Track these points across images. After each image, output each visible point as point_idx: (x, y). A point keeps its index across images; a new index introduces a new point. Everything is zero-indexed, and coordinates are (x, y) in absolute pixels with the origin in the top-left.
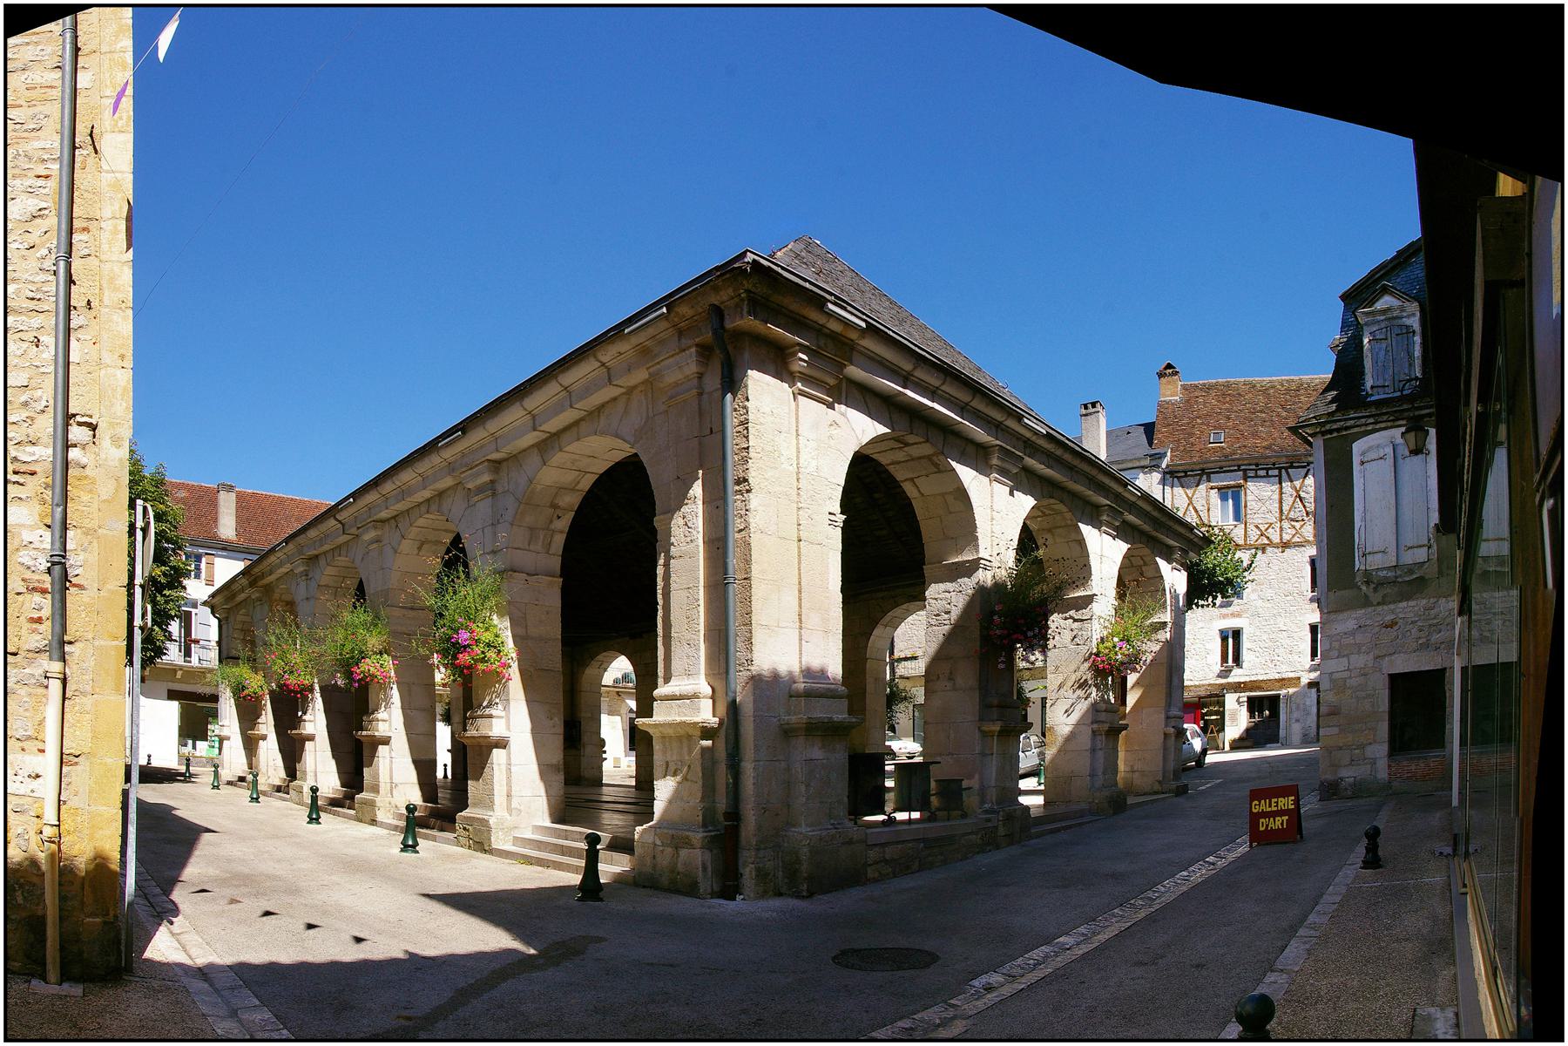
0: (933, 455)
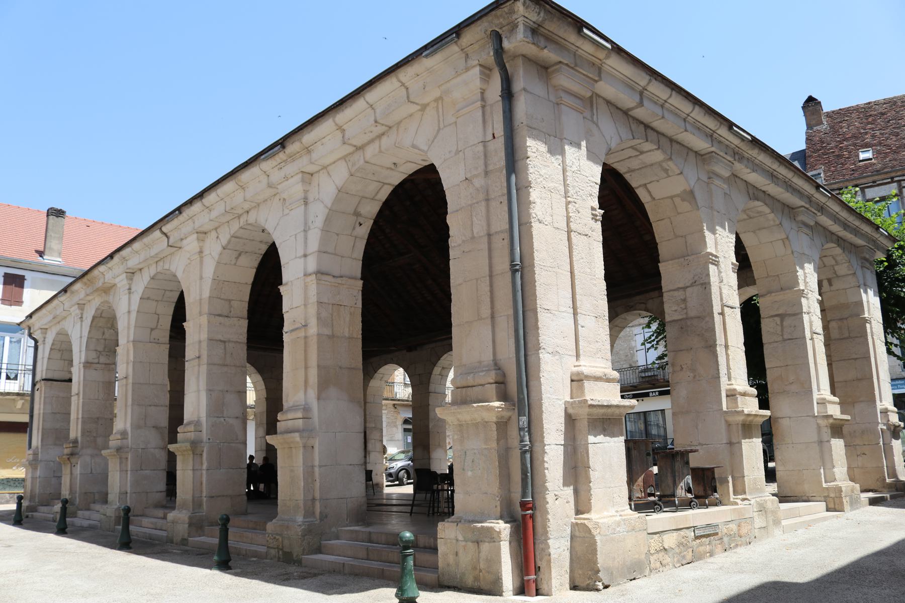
0: (662, 161)
